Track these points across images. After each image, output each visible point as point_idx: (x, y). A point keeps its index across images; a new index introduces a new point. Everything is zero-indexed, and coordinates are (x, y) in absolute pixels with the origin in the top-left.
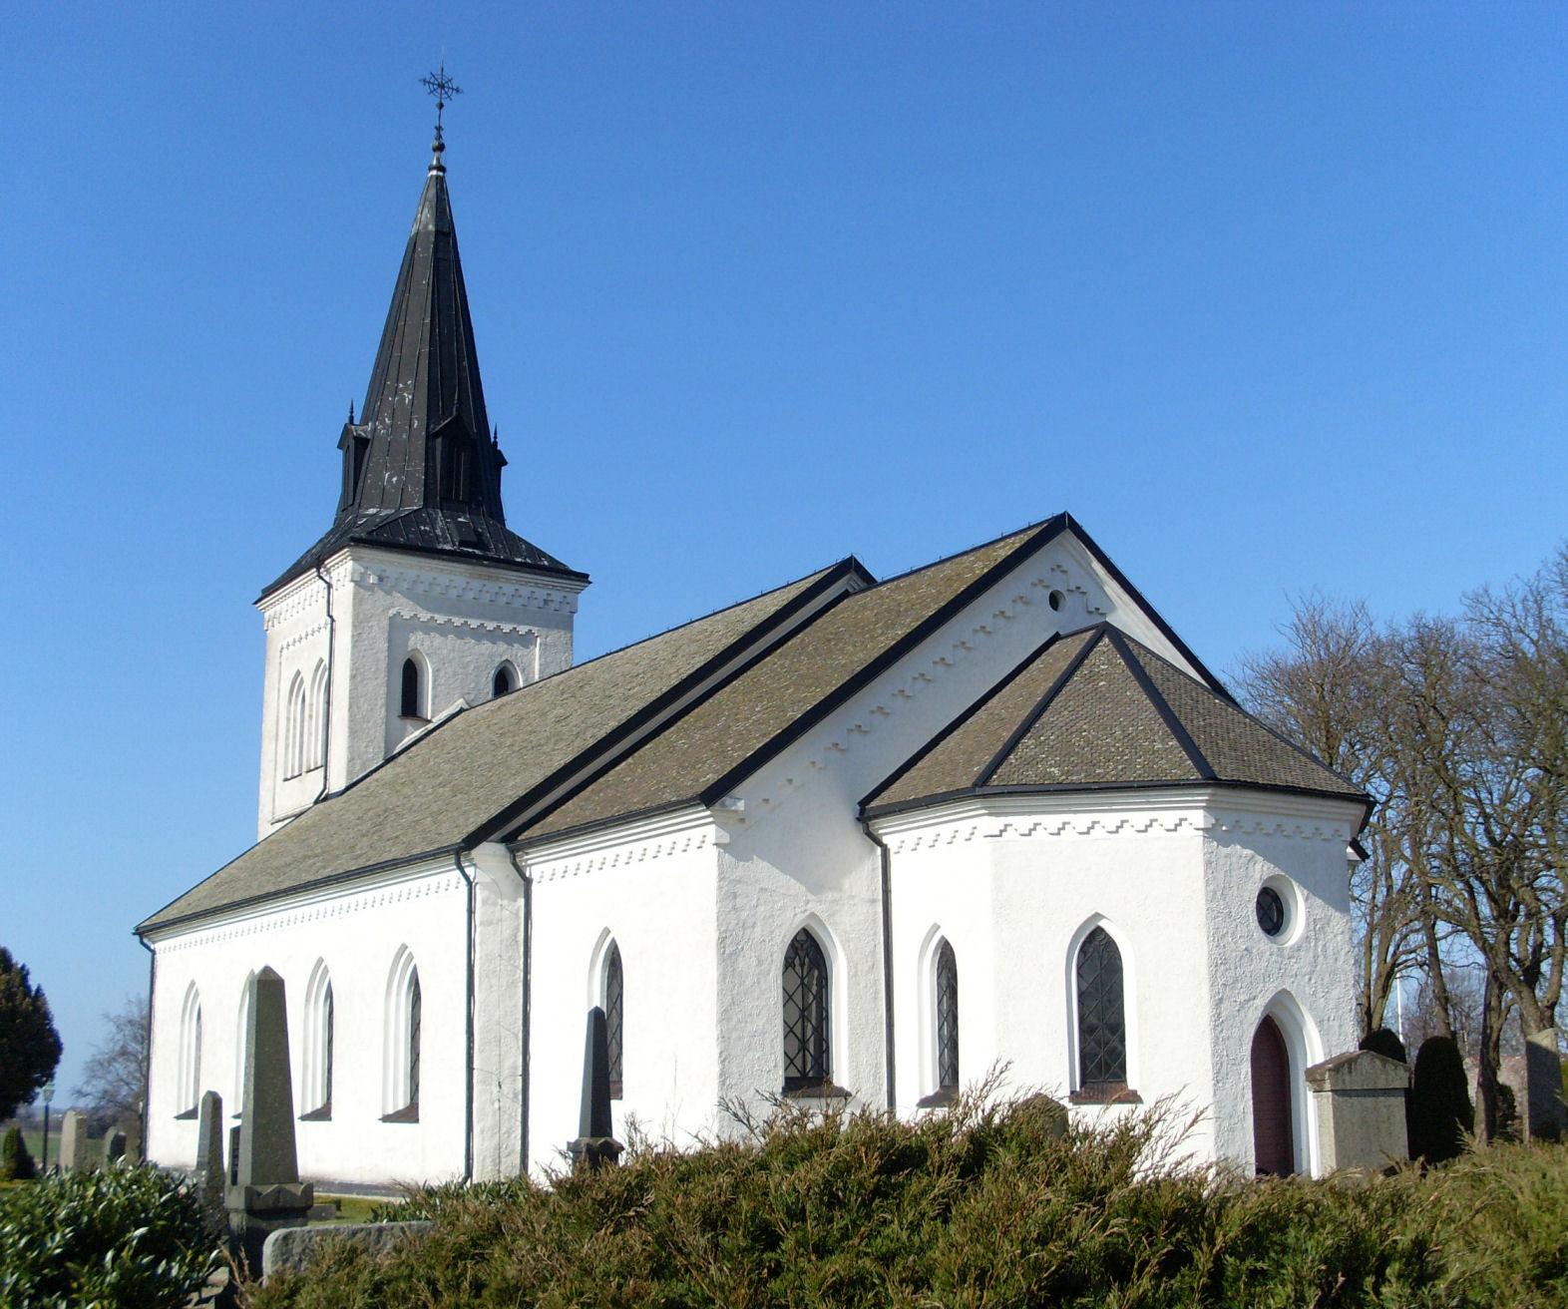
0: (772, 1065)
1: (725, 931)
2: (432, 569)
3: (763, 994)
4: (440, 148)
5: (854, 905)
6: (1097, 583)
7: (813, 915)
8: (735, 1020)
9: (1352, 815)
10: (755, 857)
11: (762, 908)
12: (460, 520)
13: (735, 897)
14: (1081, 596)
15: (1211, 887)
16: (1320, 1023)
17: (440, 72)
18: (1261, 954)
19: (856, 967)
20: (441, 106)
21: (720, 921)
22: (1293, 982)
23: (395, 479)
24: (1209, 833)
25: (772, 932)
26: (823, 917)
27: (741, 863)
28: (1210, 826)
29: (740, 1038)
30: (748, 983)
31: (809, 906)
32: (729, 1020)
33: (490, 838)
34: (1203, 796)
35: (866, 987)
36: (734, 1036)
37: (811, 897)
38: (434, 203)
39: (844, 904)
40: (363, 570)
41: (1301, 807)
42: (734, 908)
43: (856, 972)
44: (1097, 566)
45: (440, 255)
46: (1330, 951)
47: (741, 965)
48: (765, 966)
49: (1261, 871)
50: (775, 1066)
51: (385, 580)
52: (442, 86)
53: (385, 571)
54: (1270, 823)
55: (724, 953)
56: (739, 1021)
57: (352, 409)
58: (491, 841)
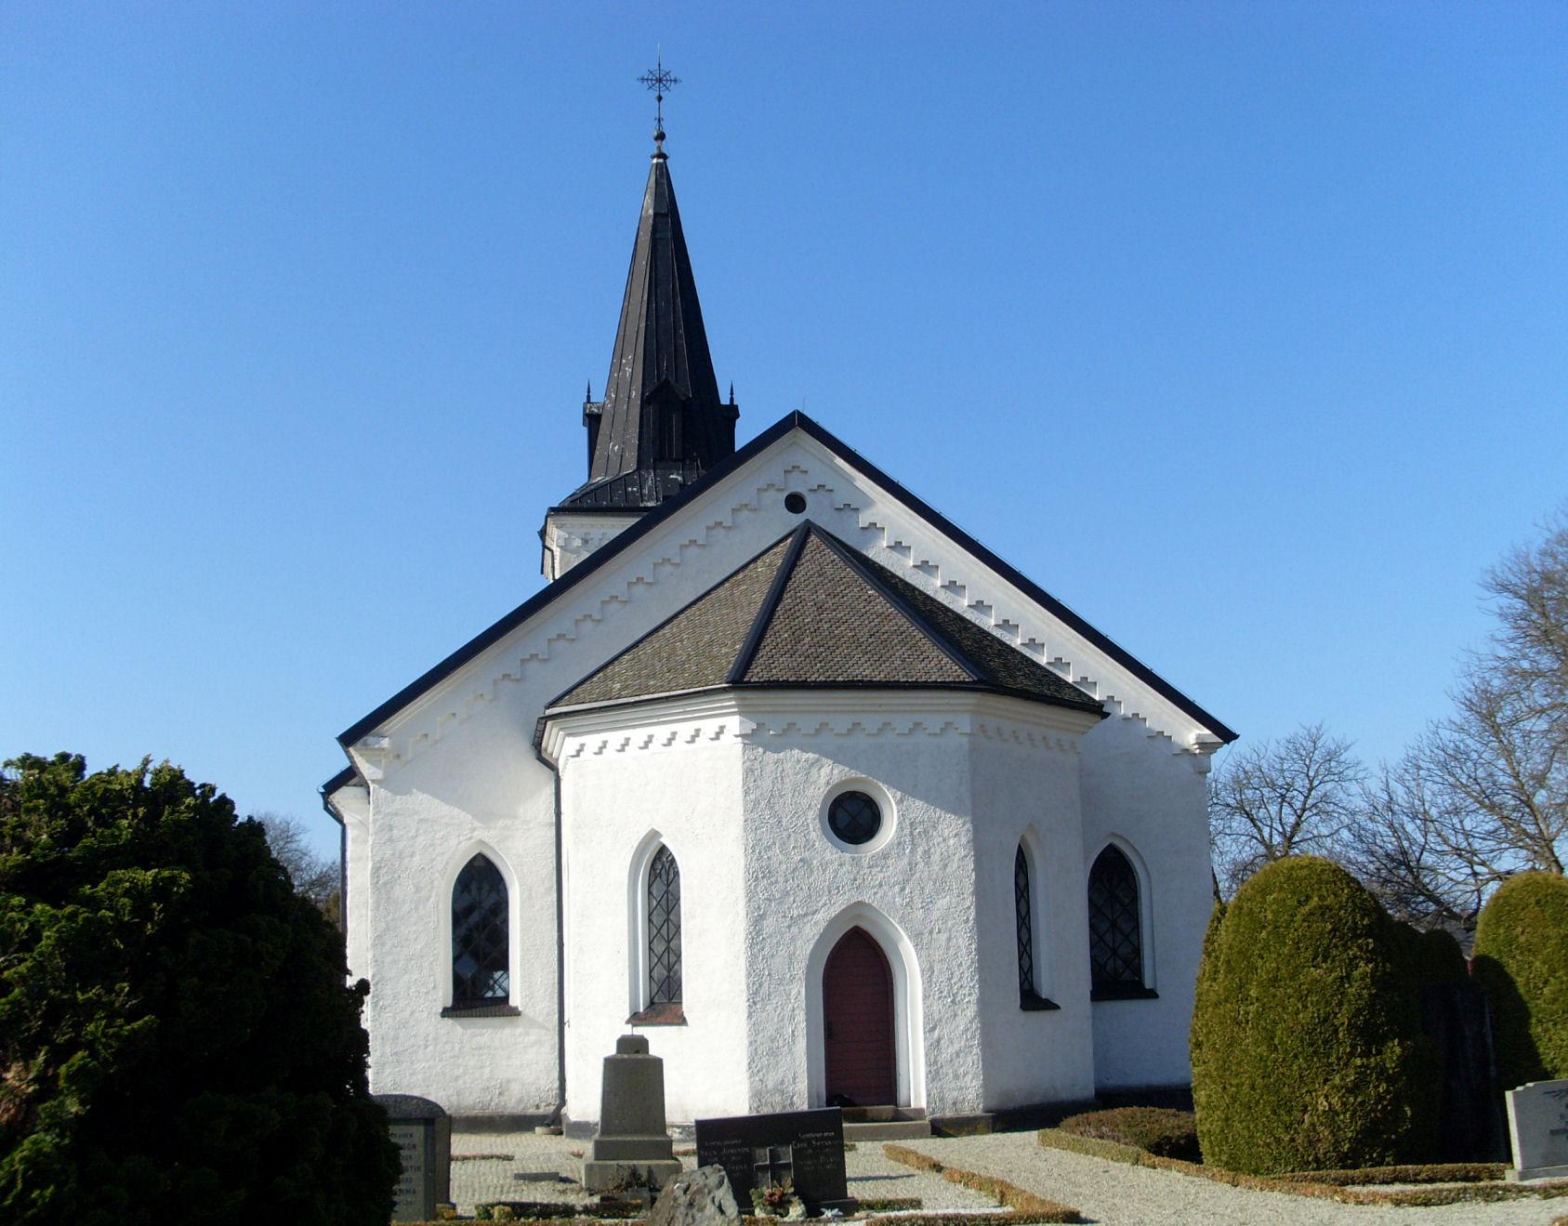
0: (431, 986)
1: (380, 861)
2: (582, 525)
3: (422, 919)
4: (661, 137)
5: (528, 830)
6: (847, 480)
7: (481, 842)
8: (389, 945)
9: (969, 705)
10: (415, 790)
11: (420, 839)
12: (672, 476)
13: (391, 830)
14: (828, 493)
15: (753, 797)
16: (917, 937)
17: (657, 67)
18: (824, 866)
19: (530, 891)
20: (660, 99)
21: (374, 852)
22: (875, 893)
23: (616, 448)
24: (749, 739)
25: (433, 860)
26: (492, 843)
27: (398, 797)
28: (750, 732)
29: (395, 962)
30: (405, 908)
31: (476, 833)
32: (383, 944)
33: (350, 783)
34: (730, 701)
35: (542, 909)
36: (388, 959)
37: (477, 824)
38: (654, 190)
39: (517, 830)
40: (567, 536)
41: (798, 702)
42: (390, 840)
43: (530, 894)
44: (840, 461)
45: (658, 235)
46: (936, 858)
47: (398, 893)
48: (424, 893)
49: (827, 777)
50: (434, 988)
51: (590, 542)
52: (660, 80)
53: (589, 534)
54: (841, 723)
55: (377, 882)
56: (394, 946)
57: (589, 388)
58: (350, 786)
